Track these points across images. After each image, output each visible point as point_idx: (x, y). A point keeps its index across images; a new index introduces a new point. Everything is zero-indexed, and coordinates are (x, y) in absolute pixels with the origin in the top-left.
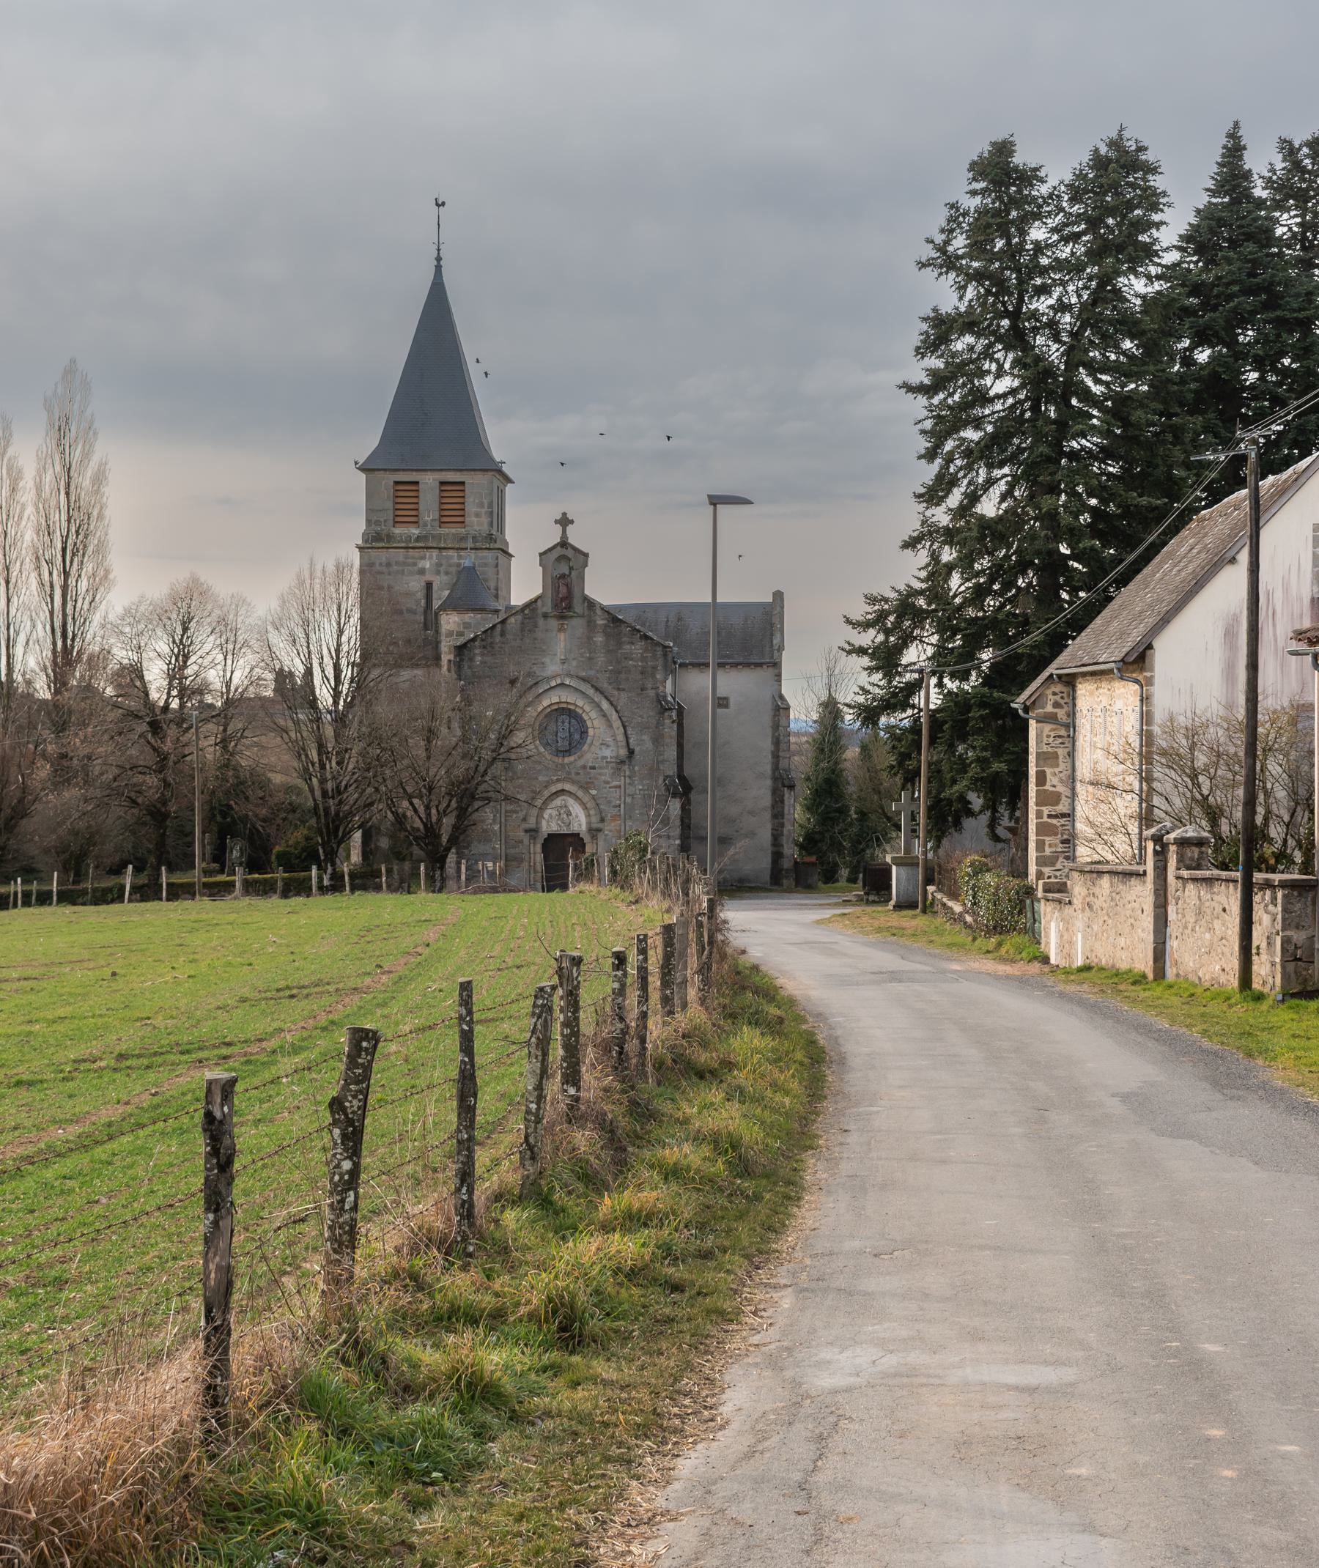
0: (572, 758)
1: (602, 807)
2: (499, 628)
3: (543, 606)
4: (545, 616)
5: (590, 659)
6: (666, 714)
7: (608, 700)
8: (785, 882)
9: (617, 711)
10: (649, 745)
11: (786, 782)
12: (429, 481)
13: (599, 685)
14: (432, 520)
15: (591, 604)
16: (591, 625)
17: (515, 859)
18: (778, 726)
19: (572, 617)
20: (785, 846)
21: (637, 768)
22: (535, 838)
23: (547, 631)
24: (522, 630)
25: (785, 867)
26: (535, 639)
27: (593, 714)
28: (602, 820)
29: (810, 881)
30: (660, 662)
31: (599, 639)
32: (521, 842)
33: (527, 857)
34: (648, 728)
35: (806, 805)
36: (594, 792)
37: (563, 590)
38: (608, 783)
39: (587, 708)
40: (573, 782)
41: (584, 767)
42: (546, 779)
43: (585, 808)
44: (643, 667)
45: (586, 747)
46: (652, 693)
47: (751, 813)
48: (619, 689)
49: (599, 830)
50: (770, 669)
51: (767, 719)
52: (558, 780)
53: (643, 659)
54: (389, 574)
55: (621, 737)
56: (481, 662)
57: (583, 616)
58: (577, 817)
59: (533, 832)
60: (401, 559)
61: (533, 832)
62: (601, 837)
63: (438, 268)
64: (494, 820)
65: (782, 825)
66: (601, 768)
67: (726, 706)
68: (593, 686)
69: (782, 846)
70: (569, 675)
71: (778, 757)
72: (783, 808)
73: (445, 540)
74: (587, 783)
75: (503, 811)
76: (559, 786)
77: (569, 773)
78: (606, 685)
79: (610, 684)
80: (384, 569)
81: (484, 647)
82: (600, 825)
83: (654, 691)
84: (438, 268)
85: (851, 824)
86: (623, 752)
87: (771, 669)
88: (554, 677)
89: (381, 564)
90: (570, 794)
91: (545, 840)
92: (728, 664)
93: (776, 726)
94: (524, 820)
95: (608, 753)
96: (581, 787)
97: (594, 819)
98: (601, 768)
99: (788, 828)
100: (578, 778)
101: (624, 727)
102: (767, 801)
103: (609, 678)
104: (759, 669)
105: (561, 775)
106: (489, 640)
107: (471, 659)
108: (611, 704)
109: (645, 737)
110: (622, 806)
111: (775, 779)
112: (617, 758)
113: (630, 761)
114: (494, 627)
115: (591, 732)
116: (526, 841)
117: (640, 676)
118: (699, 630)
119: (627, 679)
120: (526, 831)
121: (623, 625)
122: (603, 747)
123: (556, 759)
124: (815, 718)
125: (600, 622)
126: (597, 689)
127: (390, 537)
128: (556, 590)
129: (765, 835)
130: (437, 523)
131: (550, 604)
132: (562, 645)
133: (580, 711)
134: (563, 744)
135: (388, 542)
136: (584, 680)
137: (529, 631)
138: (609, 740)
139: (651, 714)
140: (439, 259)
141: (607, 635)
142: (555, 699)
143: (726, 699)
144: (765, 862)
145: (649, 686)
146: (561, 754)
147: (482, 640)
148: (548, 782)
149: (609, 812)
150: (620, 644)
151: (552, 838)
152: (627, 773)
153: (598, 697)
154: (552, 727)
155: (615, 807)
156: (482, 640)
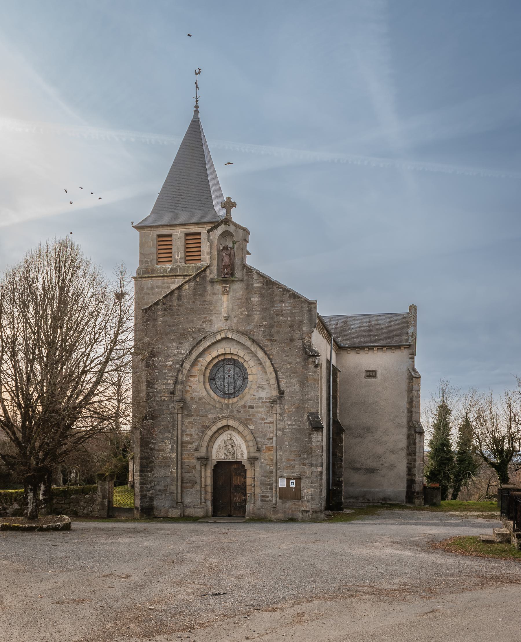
0: (235, 400)
1: (258, 439)
2: (176, 294)
3: (210, 273)
4: (212, 282)
5: (248, 316)
6: (310, 360)
7: (262, 349)
8: (416, 501)
9: (269, 359)
10: (296, 387)
11: (417, 430)
12: (178, 233)
13: (256, 338)
14: (180, 258)
15: (249, 270)
16: (249, 288)
17: (189, 481)
18: (412, 390)
19: (233, 281)
20: (417, 475)
21: (286, 407)
22: (206, 465)
23: (214, 294)
24: (194, 295)
25: (417, 490)
26: (205, 301)
27: (252, 363)
28: (259, 450)
29: (434, 501)
30: (306, 317)
31: (256, 299)
32: (194, 467)
33: (198, 480)
34: (296, 373)
35: (431, 456)
36: (252, 427)
37: (226, 259)
38: (263, 419)
39: (247, 358)
40: (235, 419)
41: (244, 406)
42: (214, 416)
43: (244, 437)
44: (292, 321)
45: (246, 390)
46: (299, 343)
47: (392, 452)
48: (271, 341)
49: (257, 459)
50: (406, 350)
51: (404, 386)
52: (223, 417)
53: (292, 314)
54: (153, 294)
55: (273, 381)
56: (163, 322)
57: (241, 281)
58: (240, 448)
59: (205, 460)
60: (160, 284)
61: (205, 460)
62: (257, 464)
63: (196, 112)
64: (172, 449)
65: (415, 460)
66: (258, 407)
67: (375, 377)
68: (250, 338)
69: (415, 475)
70: (230, 330)
71: (412, 412)
72: (415, 448)
73: (188, 270)
74: (247, 419)
75: (179, 442)
76: (224, 423)
77: (232, 411)
78: (261, 338)
79: (265, 336)
80: (150, 291)
81: (165, 310)
82: (257, 455)
83: (301, 342)
84: (196, 112)
85: (455, 466)
86: (275, 393)
87: (406, 351)
88: (219, 332)
89: (147, 288)
90: (235, 429)
91: (215, 466)
92: (376, 346)
93: (410, 390)
94: (197, 450)
95: (263, 394)
96: (241, 423)
97: (253, 449)
98: (258, 407)
99: (419, 462)
100: (238, 415)
101: (276, 372)
102: (403, 443)
103: (264, 332)
104: (398, 350)
105: (226, 413)
106: (169, 304)
107: (155, 320)
108: (265, 353)
109: (293, 380)
110: (274, 439)
111: (409, 428)
112: (270, 398)
113: (281, 401)
114: (172, 292)
115: (250, 377)
116: (198, 467)
117: (289, 330)
118: (358, 329)
119: (278, 332)
120: (198, 459)
121: (275, 287)
122: (260, 390)
123: (223, 400)
124: (435, 413)
125: (256, 285)
126: (253, 341)
127: (153, 270)
128: (220, 259)
129: (402, 467)
130: (183, 261)
131: (215, 271)
132: (225, 305)
133: (241, 361)
134: (229, 389)
135: (152, 274)
136: (243, 333)
137: (200, 295)
138: (264, 383)
139: (299, 360)
140: (197, 107)
141: (262, 296)
142: (221, 351)
143: (375, 372)
144: (402, 487)
145: (297, 337)
146: (227, 397)
147: (164, 304)
148: (215, 418)
149: (264, 443)
150: (272, 302)
151: (220, 465)
152: (279, 411)
153: (254, 348)
154: (220, 375)
155: (269, 439)
156: (164, 304)
